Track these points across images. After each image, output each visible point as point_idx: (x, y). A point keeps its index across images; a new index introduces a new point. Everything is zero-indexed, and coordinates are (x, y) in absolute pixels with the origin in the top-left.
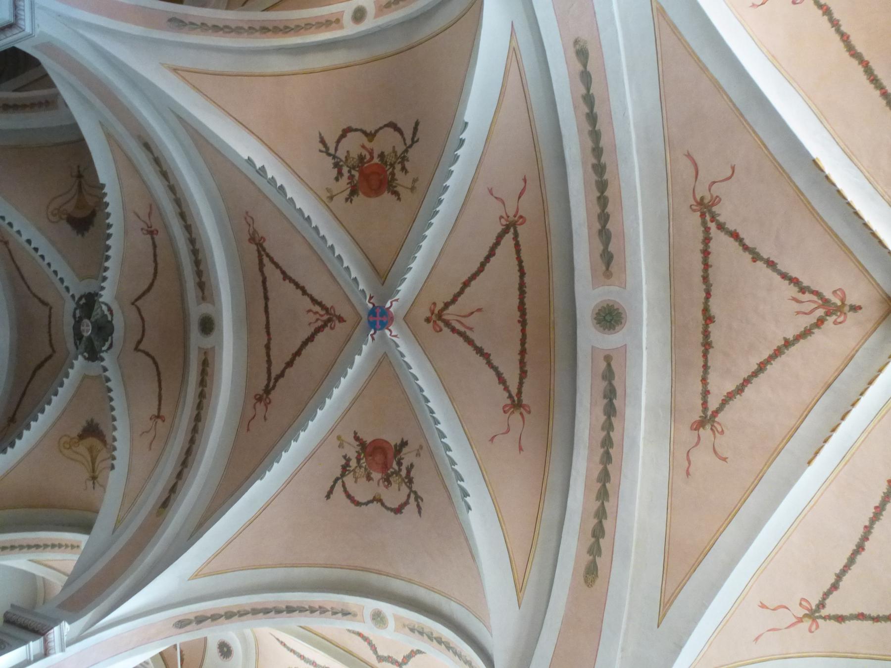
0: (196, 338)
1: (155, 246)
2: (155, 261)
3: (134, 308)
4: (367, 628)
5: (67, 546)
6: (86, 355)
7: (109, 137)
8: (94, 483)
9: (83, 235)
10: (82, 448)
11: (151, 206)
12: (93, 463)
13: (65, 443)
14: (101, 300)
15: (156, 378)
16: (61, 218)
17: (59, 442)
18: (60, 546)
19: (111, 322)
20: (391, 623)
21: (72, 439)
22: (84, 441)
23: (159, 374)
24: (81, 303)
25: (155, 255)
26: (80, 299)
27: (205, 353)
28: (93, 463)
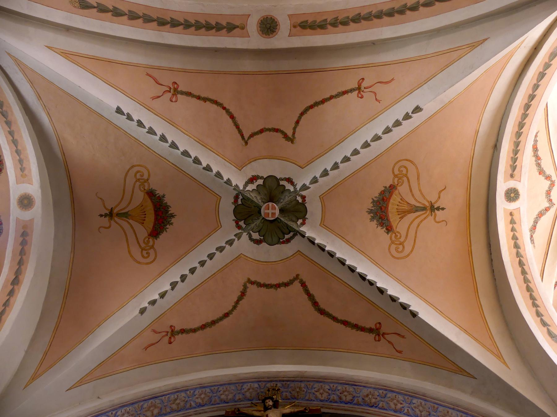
0: (282, 40)
1: (189, 94)
2: (205, 100)
3: (251, 142)
4: (521, 204)
5: (513, 230)
6: (300, 221)
7: (66, 55)
8: (438, 209)
9: (172, 216)
10: (401, 226)
11: (148, 74)
12: (416, 209)
13: (397, 252)
14: (241, 188)
15: (321, 106)
16: (152, 247)
17: (398, 258)
18: (518, 255)
19: (265, 179)
20: (512, 184)
21: (393, 242)
22: (394, 225)
23: (317, 104)
24: (244, 226)
25: (199, 98)
26: (239, 227)
27: (295, 27)
28: (416, 209)
